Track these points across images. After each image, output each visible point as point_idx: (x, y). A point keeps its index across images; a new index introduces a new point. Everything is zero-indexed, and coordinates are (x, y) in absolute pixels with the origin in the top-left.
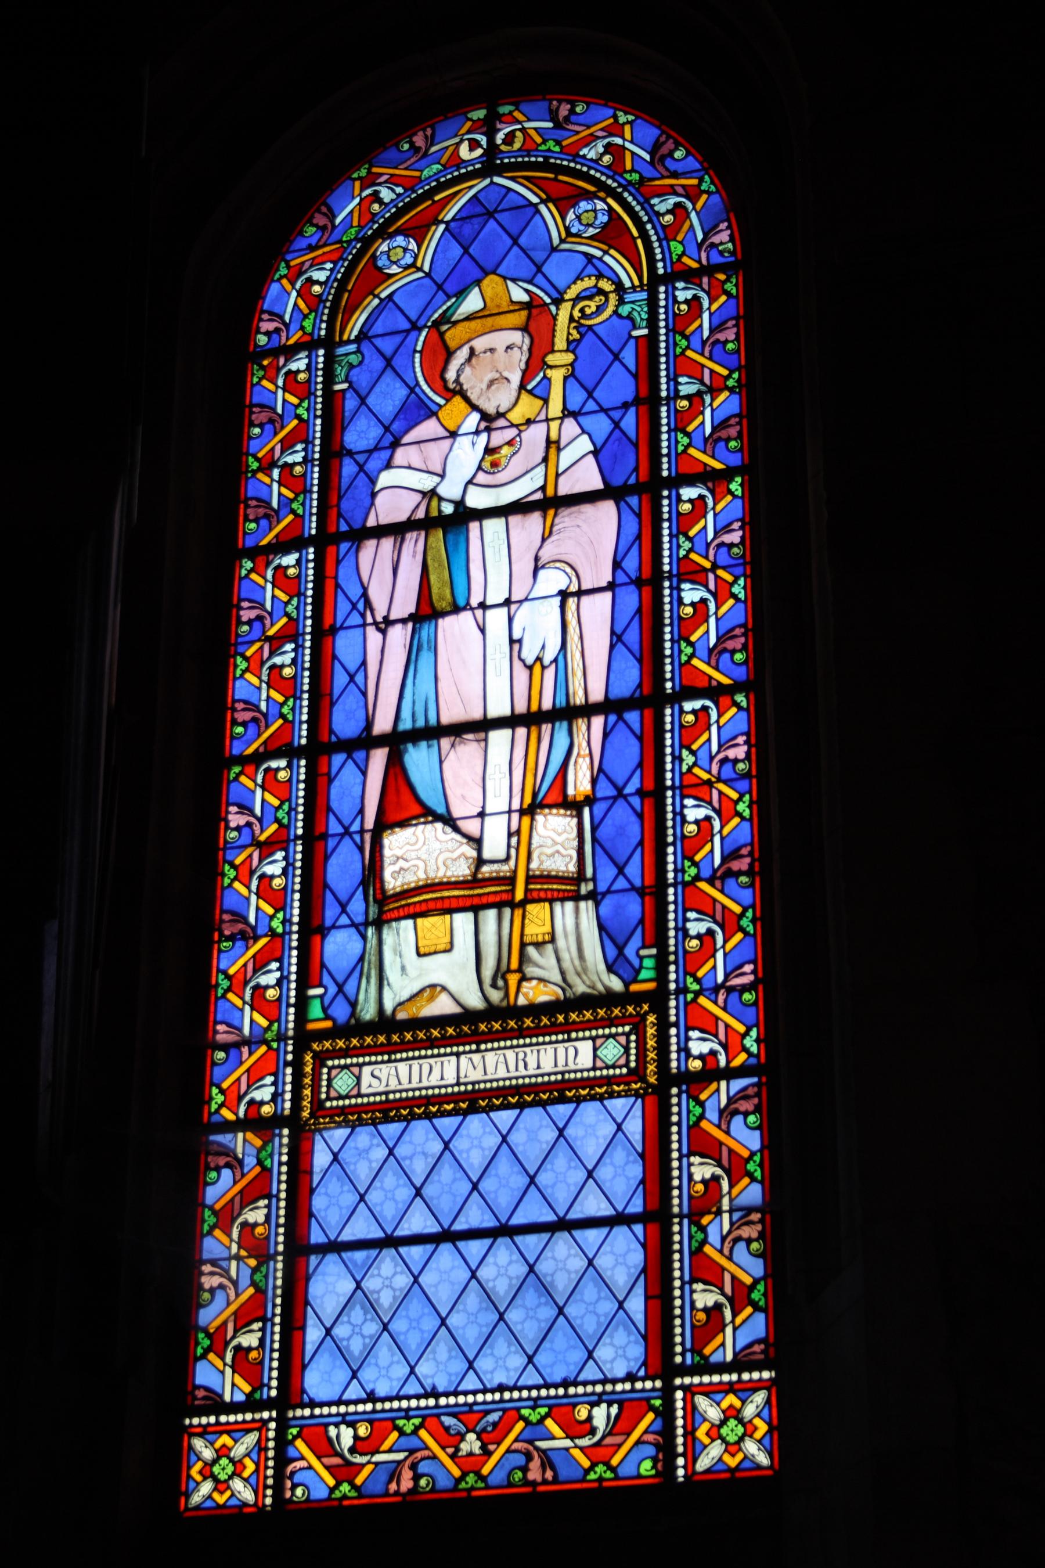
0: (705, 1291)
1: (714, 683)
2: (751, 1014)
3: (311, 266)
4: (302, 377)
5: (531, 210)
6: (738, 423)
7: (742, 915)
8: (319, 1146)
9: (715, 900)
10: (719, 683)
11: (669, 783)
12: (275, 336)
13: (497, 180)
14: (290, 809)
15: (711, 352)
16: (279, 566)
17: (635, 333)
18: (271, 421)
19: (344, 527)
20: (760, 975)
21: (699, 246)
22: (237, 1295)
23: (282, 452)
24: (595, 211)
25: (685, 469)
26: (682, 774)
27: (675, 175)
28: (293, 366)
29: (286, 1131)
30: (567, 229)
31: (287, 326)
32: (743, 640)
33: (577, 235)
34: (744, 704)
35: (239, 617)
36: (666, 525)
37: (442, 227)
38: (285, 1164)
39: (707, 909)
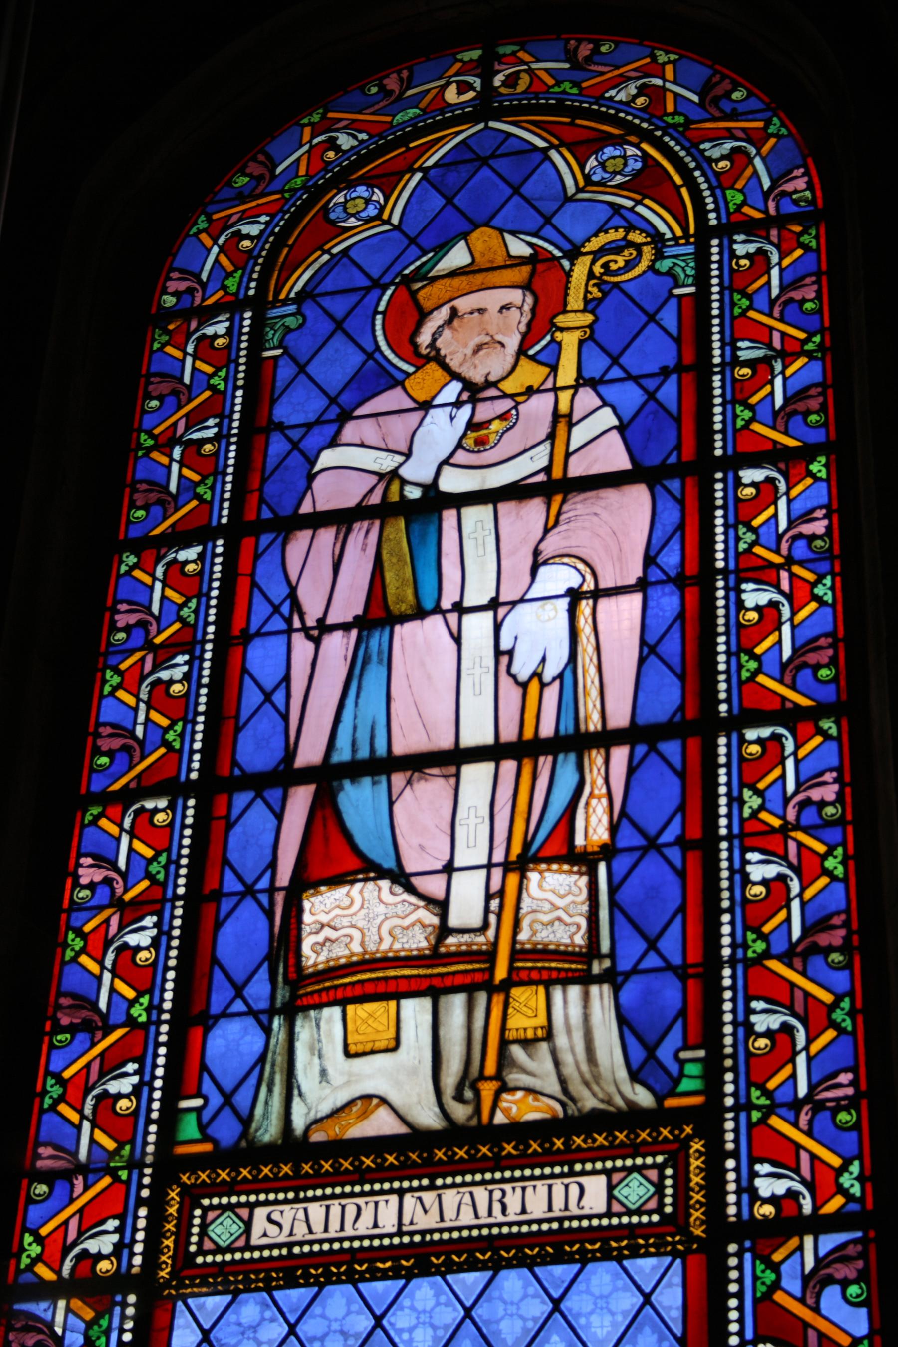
3: (240, 219)
7: (835, 1005)
8: (182, 1319)
10: (796, 705)
11: (723, 831)
13: (492, 124)
14: (169, 861)
17: (677, 292)
24: (624, 157)
27: (734, 116)
30: (587, 178)
31: (204, 286)
34: (834, 732)
37: (418, 176)
39: (782, 997)
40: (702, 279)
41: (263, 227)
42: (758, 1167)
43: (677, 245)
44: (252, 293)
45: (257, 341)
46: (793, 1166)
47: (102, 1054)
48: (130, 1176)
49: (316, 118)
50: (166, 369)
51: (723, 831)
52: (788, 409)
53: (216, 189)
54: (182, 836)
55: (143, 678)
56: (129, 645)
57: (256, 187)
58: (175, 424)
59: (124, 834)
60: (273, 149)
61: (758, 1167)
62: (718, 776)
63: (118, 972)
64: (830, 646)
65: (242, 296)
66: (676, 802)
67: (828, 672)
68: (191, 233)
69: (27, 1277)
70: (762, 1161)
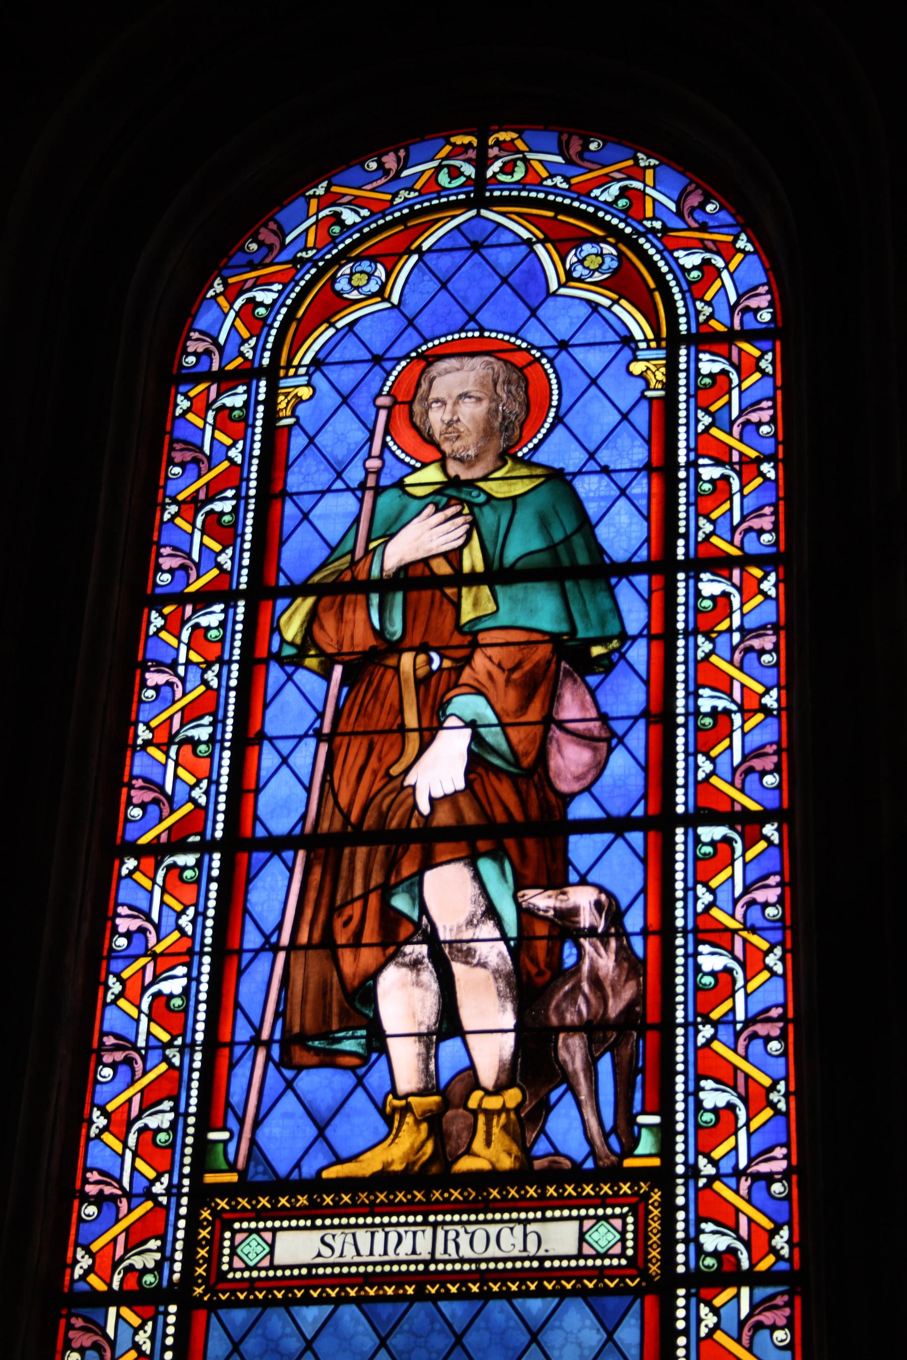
0: (713, 954)
1: (737, 808)
2: (771, 676)
3: (254, 286)
4: (177, 1002)
5: (524, 249)
6: (786, 1304)
7: (773, 1088)
8: (216, 1334)
9: (736, 1068)
10: (743, 807)
11: (680, 1235)
12: (204, 358)
13: (484, 213)
14: (197, 914)
15: (741, 434)
16: (174, 865)
17: (649, 394)
18: (196, 461)
19: (283, 581)
20: (794, 1161)
21: (732, 309)
22: (185, 694)
23: (182, 725)
24: (601, 255)
25: (707, 802)
26: (696, 914)
27: (703, 228)
28: (204, 621)
29: (173, 1308)
30: (569, 274)
31: (221, 349)
32: (775, 759)
33: (580, 280)
35: (115, 927)
36: (680, 1079)
37: (415, 258)
38: (228, 749)
39: (729, 1078)
40: (671, 384)
41: (276, 296)
42: (703, 1083)
43: (649, 348)
44: (176, 1277)
45: (271, 403)
46: (732, 1084)
47: (207, 484)
48: (169, 1201)
49: (320, 191)
50: (148, 773)
51: (680, 1235)
52: (745, 525)
53: (231, 253)
54: (183, 1155)
55: (144, 989)
56: (131, 952)
57: (266, 256)
58: (171, 718)
59: (127, 1151)
60: (282, 216)
61: (703, 1083)
62: (675, 1143)
63: (153, 1016)
64: (775, 753)
65: (256, 365)
66: (641, 791)
67: (776, 912)
68: (208, 296)
69: (81, 1286)
70: (706, 1220)
